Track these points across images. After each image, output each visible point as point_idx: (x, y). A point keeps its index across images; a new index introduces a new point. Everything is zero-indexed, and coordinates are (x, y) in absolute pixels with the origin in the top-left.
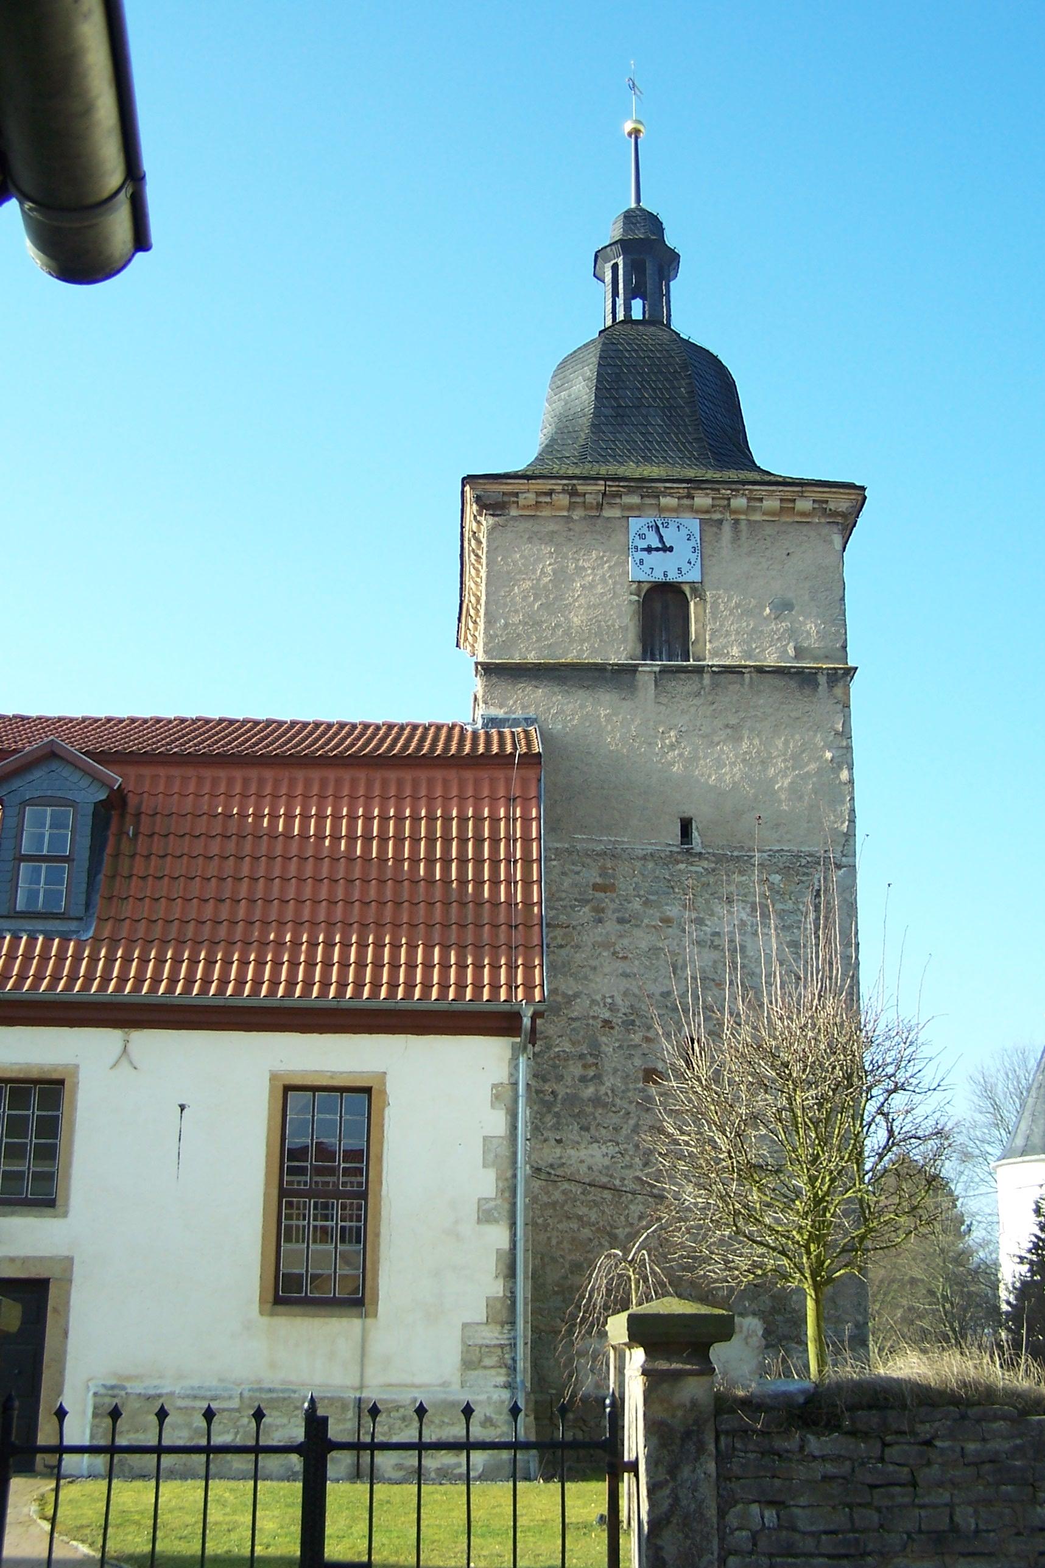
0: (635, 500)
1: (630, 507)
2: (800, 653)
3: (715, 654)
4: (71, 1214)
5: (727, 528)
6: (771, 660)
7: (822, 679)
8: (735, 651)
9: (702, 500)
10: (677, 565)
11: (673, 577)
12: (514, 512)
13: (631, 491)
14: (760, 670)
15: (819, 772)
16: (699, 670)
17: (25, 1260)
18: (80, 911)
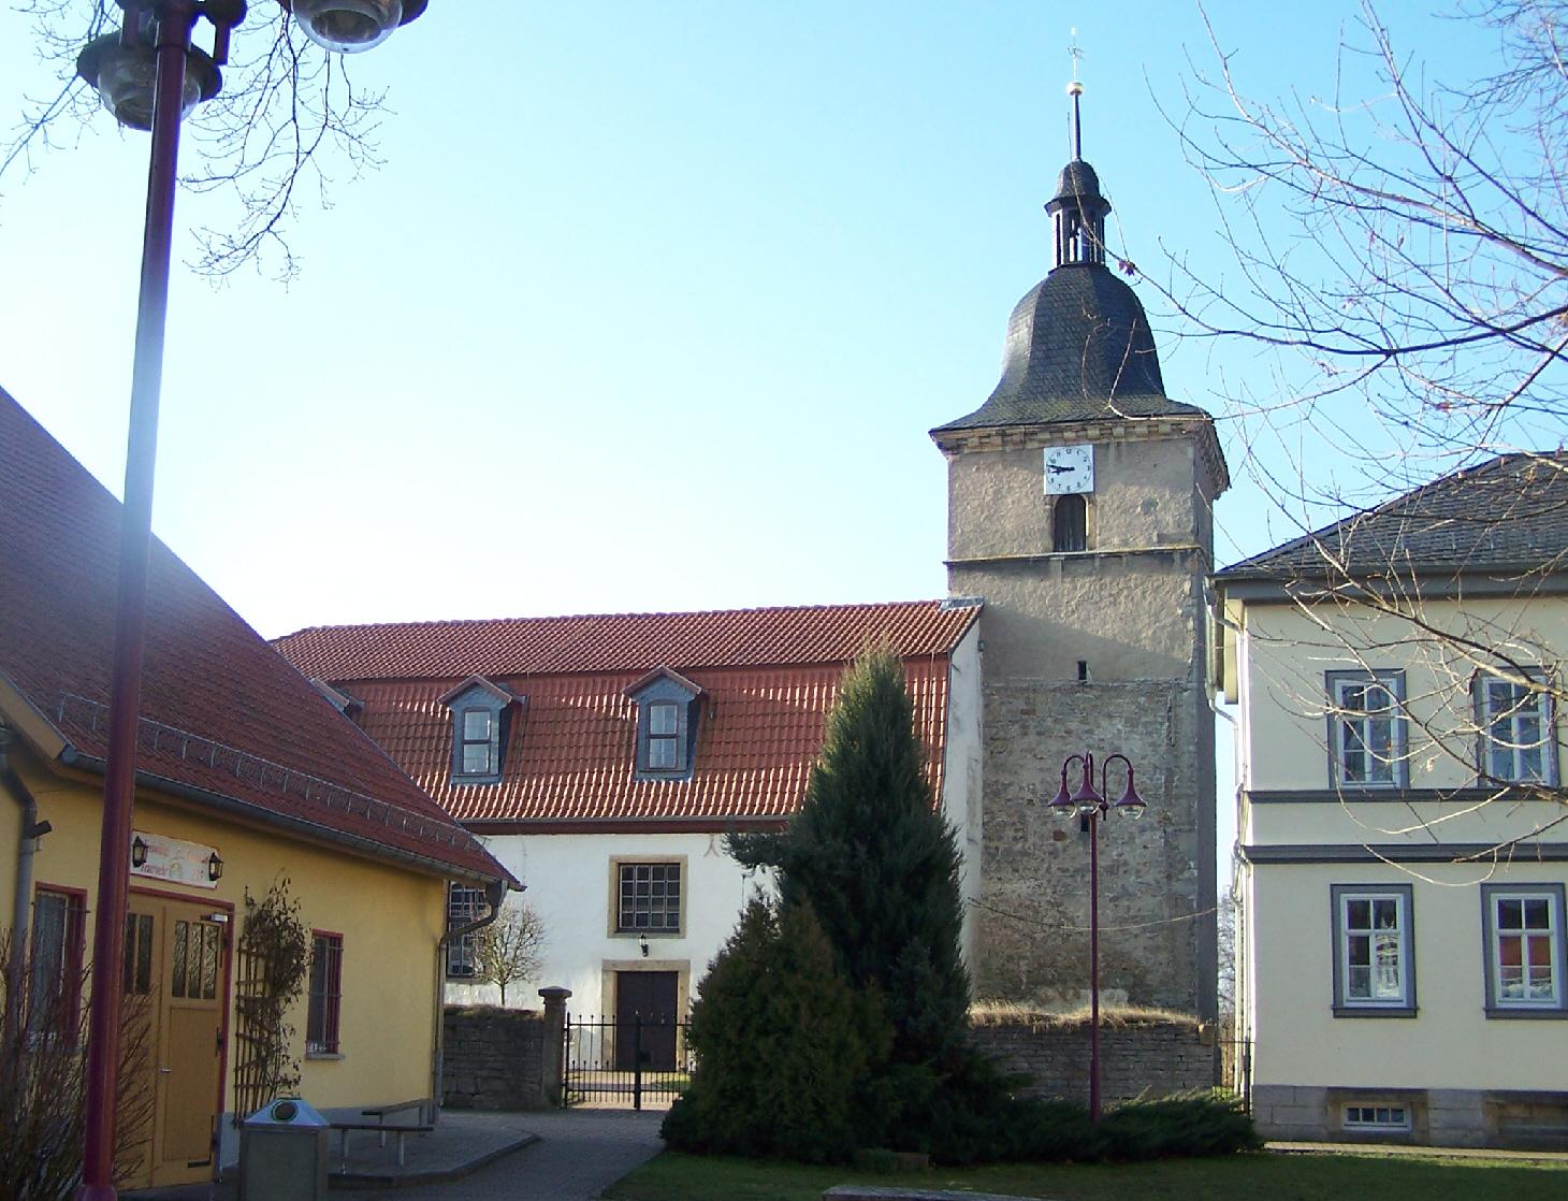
0: (1047, 436)
1: (1044, 441)
2: (1161, 539)
3: (1103, 544)
4: (688, 936)
5: (1112, 449)
6: (1141, 546)
7: (1177, 557)
8: (1116, 541)
9: (1093, 432)
10: (1079, 480)
11: (1074, 490)
12: (966, 451)
13: (1043, 430)
14: (1133, 553)
15: (1174, 623)
16: (1092, 556)
17: (665, 962)
18: (495, 771)
